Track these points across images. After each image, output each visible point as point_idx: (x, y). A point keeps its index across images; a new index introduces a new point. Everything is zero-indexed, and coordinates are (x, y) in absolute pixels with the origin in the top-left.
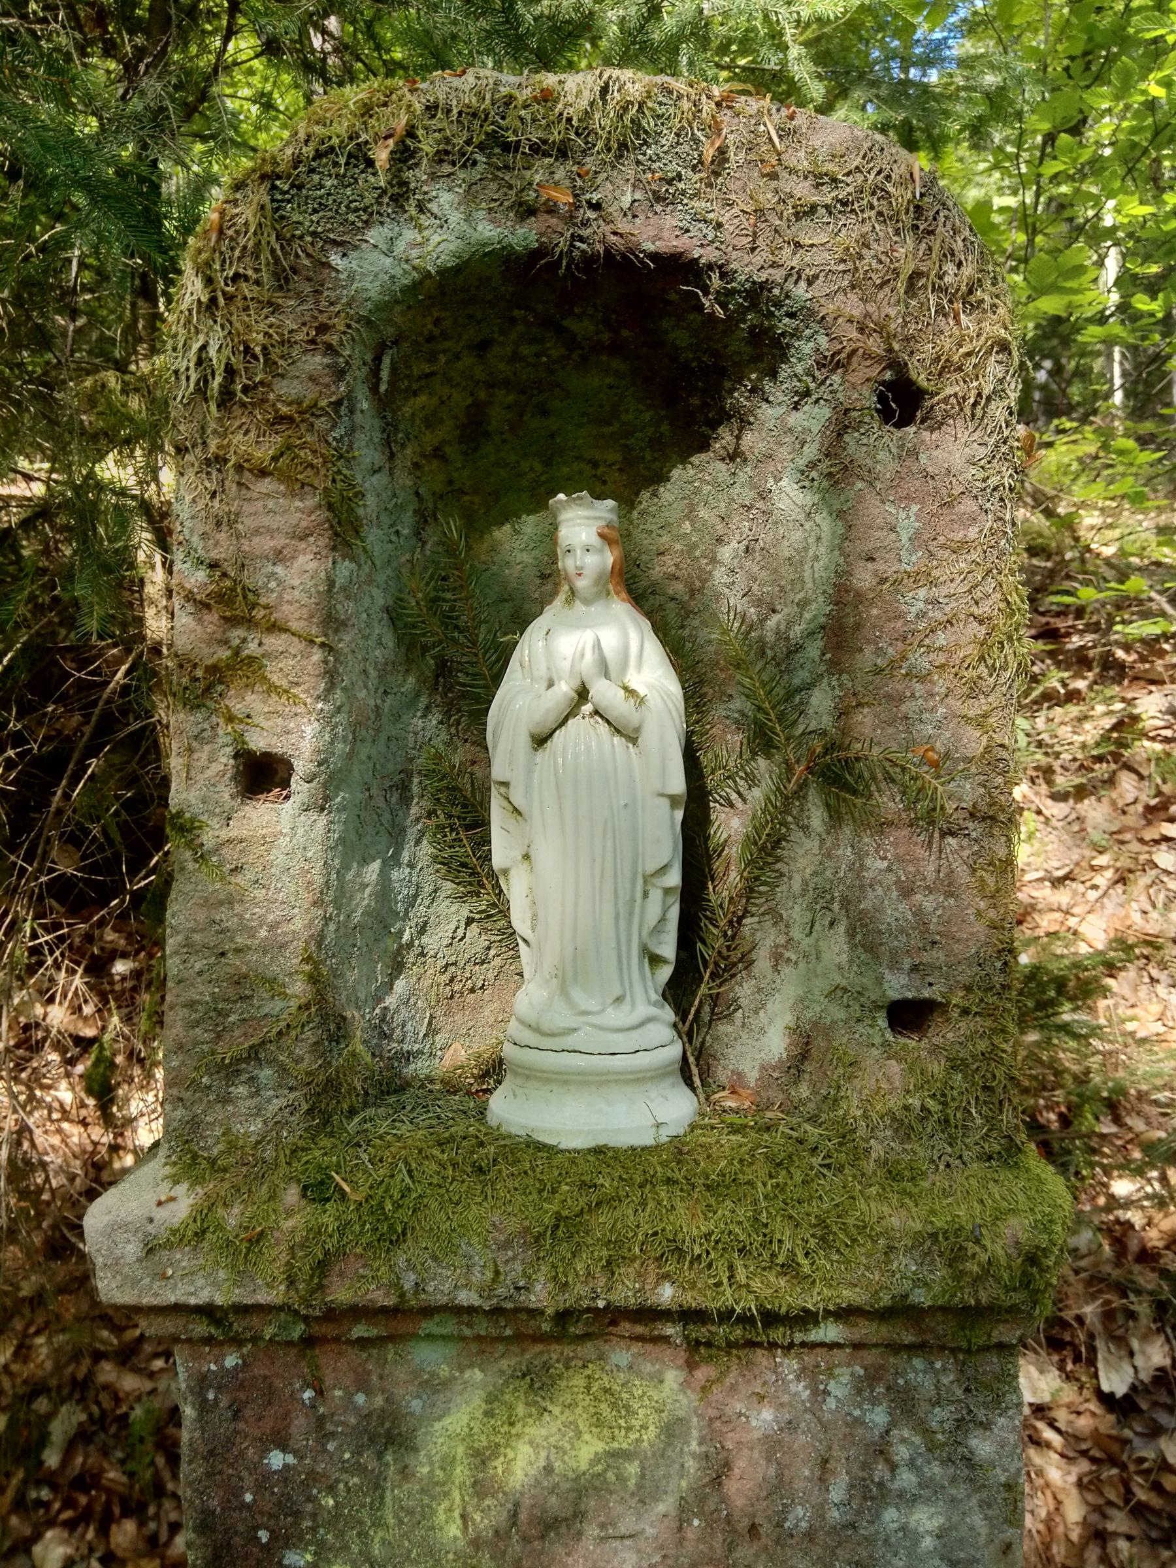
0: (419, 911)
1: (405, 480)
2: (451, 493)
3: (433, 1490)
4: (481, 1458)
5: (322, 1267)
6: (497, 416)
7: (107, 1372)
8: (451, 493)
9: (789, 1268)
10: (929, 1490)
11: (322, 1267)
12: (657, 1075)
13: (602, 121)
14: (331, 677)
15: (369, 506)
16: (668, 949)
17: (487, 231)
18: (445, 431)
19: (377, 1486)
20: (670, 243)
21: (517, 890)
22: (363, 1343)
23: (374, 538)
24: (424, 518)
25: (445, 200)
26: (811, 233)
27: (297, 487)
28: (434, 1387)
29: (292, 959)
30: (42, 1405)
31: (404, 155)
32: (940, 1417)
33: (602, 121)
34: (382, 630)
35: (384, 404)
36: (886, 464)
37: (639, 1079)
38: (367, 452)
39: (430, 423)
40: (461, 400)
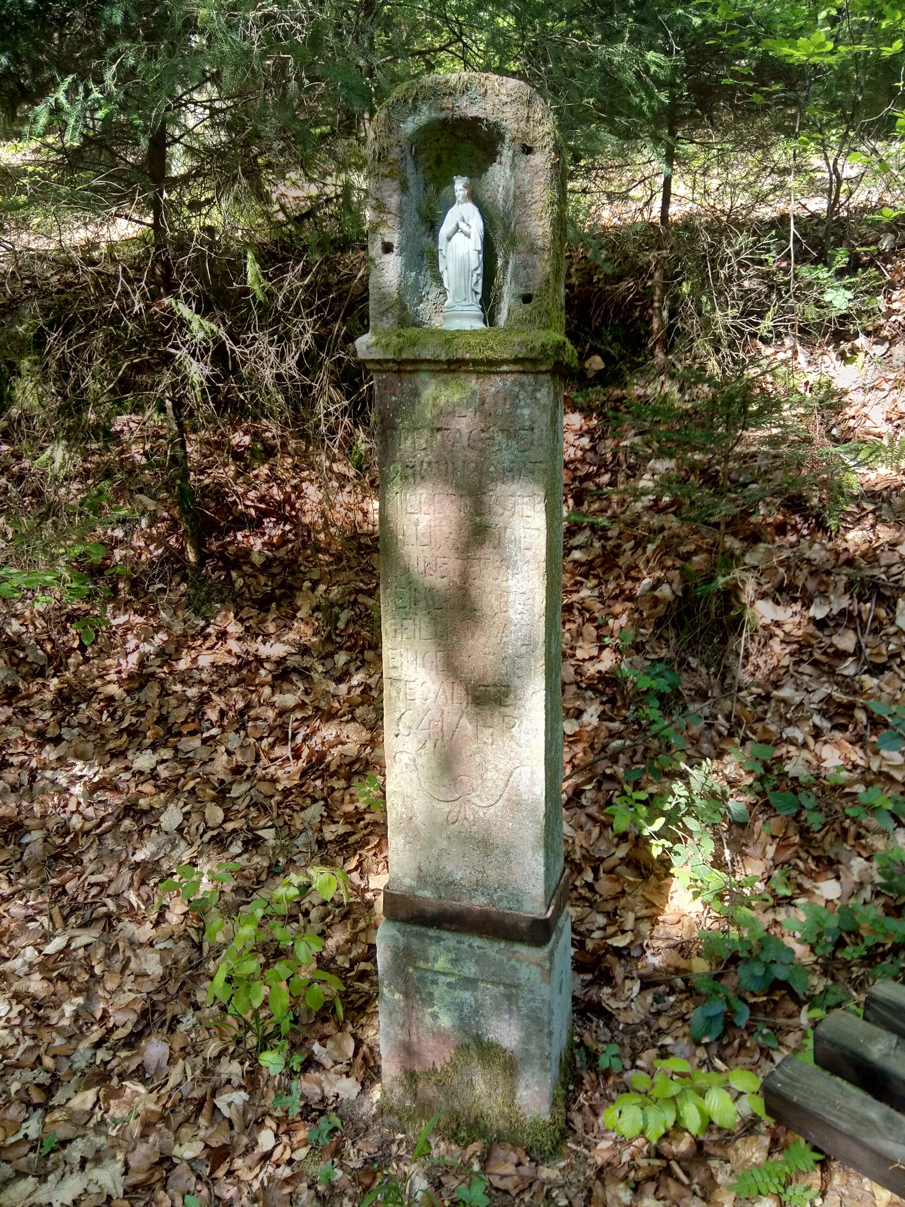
0: (427, 288)
1: (421, 176)
2: (434, 178)
3: (425, 405)
4: (435, 399)
5: (400, 350)
6: (444, 157)
7: (362, 598)
8: (434, 178)
9: (492, 349)
10: (527, 405)
11: (400, 350)
12: (475, 317)
13: (459, 87)
14: (401, 224)
15: (411, 183)
16: (479, 289)
17: (434, 115)
18: (431, 162)
19: (413, 404)
20: (474, 114)
21: (445, 277)
22: (410, 372)
23: (412, 191)
24: (426, 185)
25: (424, 108)
26: (507, 109)
27: (394, 179)
28: (425, 384)
29: (394, 289)
30: (336, 610)
31: (415, 99)
32: (530, 389)
33: (459, 87)
34: (415, 213)
35: (415, 157)
36: (523, 164)
37: (469, 317)
38: (410, 169)
39: (427, 160)
40: (434, 154)
